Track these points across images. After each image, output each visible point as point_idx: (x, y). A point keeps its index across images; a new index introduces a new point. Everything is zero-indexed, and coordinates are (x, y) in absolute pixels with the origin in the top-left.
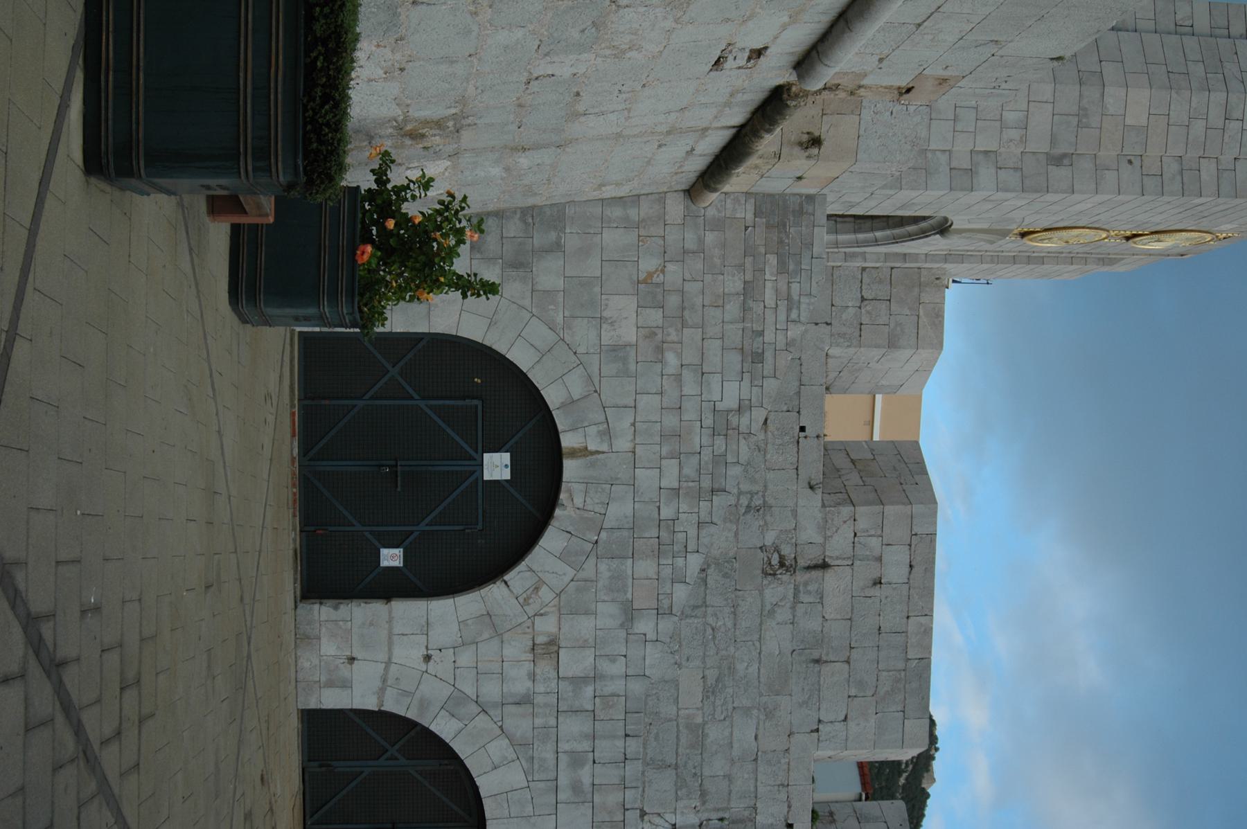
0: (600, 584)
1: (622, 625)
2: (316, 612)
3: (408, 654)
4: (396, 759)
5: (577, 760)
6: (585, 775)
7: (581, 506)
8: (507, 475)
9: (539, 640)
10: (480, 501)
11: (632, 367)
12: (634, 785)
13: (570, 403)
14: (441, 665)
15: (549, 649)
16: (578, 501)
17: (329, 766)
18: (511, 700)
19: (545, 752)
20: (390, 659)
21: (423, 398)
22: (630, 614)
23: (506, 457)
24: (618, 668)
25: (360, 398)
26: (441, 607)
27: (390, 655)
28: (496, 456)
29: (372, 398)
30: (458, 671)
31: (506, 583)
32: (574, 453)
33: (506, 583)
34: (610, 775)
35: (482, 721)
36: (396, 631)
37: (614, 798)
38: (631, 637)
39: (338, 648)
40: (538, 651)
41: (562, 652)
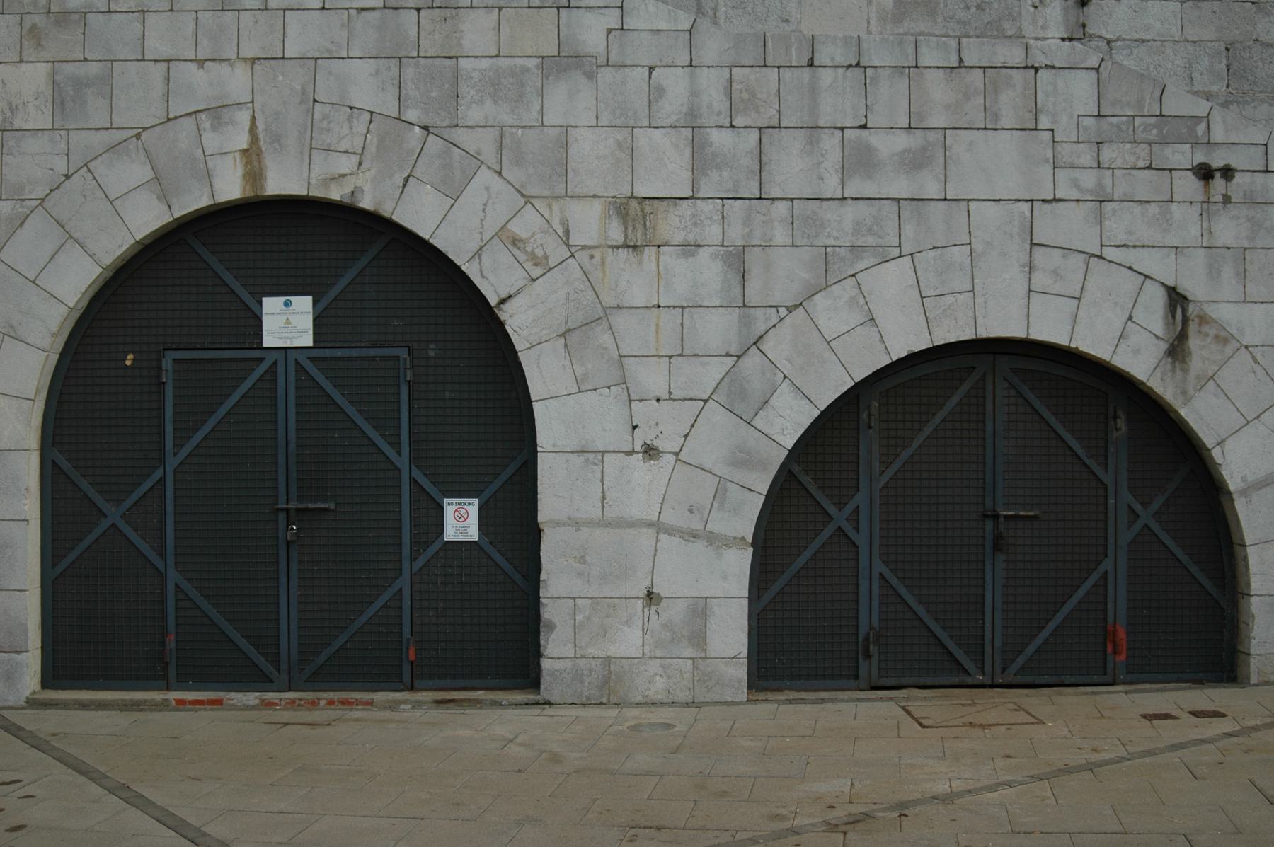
0: (508, 119)
1: (590, 76)
2: (559, 665)
3: (642, 489)
4: (857, 510)
5: (860, 162)
6: (887, 145)
7: (355, 159)
8: (304, 304)
9: (617, 235)
10: (354, 353)
11: (93, 69)
12: (911, 50)
13: (161, 185)
14: (666, 426)
15: (636, 218)
16: (345, 164)
17: (867, 639)
18: (737, 291)
19: (842, 223)
20: (650, 525)
21: (162, 460)
22: (566, 61)
23: (271, 306)
24: (675, 83)
25: (163, 577)
26: (550, 427)
27: (647, 520)
28: (269, 324)
29: (163, 555)
30: (677, 393)
31: (503, 301)
32: (254, 175)
33: (503, 301)
34: (890, 100)
35: (778, 346)
36: (596, 512)
37: (937, 88)
38: (613, 58)
39: (628, 623)
40: (639, 237)
41: (641, 191)
